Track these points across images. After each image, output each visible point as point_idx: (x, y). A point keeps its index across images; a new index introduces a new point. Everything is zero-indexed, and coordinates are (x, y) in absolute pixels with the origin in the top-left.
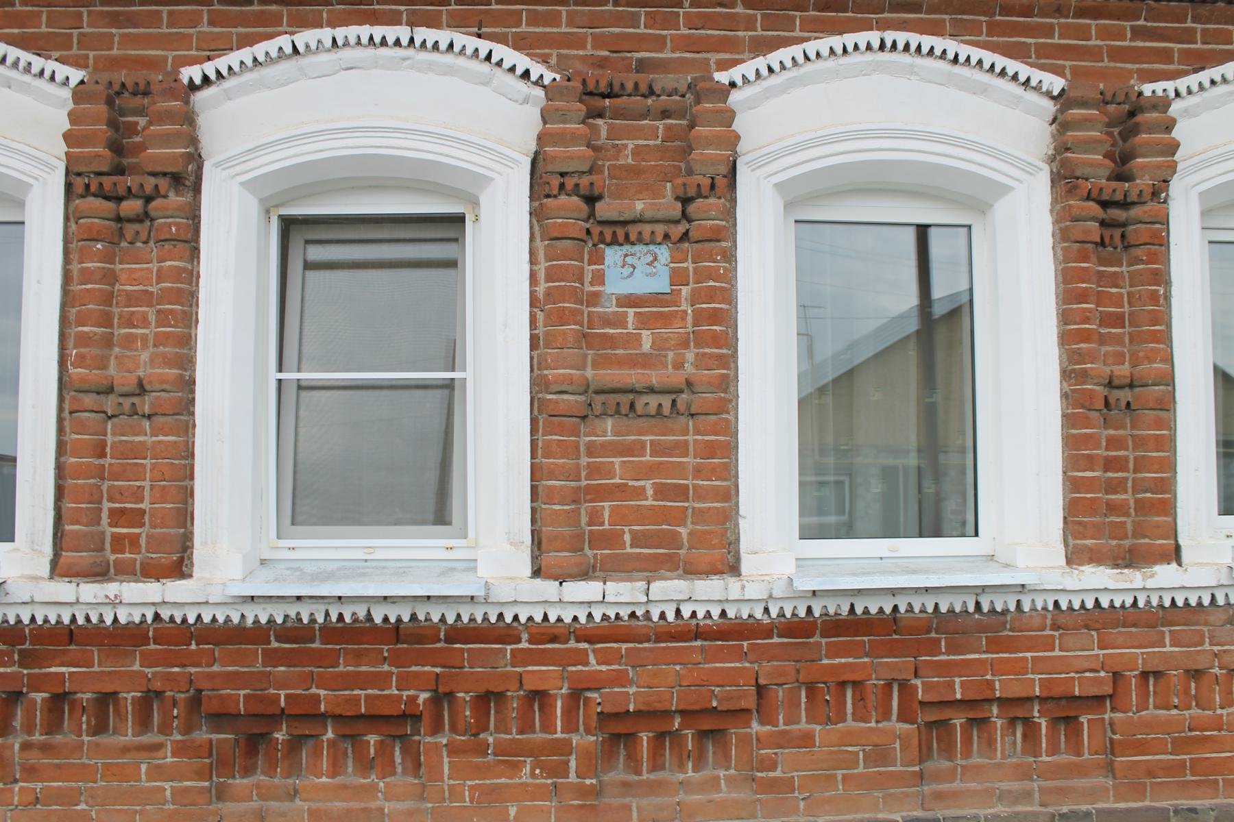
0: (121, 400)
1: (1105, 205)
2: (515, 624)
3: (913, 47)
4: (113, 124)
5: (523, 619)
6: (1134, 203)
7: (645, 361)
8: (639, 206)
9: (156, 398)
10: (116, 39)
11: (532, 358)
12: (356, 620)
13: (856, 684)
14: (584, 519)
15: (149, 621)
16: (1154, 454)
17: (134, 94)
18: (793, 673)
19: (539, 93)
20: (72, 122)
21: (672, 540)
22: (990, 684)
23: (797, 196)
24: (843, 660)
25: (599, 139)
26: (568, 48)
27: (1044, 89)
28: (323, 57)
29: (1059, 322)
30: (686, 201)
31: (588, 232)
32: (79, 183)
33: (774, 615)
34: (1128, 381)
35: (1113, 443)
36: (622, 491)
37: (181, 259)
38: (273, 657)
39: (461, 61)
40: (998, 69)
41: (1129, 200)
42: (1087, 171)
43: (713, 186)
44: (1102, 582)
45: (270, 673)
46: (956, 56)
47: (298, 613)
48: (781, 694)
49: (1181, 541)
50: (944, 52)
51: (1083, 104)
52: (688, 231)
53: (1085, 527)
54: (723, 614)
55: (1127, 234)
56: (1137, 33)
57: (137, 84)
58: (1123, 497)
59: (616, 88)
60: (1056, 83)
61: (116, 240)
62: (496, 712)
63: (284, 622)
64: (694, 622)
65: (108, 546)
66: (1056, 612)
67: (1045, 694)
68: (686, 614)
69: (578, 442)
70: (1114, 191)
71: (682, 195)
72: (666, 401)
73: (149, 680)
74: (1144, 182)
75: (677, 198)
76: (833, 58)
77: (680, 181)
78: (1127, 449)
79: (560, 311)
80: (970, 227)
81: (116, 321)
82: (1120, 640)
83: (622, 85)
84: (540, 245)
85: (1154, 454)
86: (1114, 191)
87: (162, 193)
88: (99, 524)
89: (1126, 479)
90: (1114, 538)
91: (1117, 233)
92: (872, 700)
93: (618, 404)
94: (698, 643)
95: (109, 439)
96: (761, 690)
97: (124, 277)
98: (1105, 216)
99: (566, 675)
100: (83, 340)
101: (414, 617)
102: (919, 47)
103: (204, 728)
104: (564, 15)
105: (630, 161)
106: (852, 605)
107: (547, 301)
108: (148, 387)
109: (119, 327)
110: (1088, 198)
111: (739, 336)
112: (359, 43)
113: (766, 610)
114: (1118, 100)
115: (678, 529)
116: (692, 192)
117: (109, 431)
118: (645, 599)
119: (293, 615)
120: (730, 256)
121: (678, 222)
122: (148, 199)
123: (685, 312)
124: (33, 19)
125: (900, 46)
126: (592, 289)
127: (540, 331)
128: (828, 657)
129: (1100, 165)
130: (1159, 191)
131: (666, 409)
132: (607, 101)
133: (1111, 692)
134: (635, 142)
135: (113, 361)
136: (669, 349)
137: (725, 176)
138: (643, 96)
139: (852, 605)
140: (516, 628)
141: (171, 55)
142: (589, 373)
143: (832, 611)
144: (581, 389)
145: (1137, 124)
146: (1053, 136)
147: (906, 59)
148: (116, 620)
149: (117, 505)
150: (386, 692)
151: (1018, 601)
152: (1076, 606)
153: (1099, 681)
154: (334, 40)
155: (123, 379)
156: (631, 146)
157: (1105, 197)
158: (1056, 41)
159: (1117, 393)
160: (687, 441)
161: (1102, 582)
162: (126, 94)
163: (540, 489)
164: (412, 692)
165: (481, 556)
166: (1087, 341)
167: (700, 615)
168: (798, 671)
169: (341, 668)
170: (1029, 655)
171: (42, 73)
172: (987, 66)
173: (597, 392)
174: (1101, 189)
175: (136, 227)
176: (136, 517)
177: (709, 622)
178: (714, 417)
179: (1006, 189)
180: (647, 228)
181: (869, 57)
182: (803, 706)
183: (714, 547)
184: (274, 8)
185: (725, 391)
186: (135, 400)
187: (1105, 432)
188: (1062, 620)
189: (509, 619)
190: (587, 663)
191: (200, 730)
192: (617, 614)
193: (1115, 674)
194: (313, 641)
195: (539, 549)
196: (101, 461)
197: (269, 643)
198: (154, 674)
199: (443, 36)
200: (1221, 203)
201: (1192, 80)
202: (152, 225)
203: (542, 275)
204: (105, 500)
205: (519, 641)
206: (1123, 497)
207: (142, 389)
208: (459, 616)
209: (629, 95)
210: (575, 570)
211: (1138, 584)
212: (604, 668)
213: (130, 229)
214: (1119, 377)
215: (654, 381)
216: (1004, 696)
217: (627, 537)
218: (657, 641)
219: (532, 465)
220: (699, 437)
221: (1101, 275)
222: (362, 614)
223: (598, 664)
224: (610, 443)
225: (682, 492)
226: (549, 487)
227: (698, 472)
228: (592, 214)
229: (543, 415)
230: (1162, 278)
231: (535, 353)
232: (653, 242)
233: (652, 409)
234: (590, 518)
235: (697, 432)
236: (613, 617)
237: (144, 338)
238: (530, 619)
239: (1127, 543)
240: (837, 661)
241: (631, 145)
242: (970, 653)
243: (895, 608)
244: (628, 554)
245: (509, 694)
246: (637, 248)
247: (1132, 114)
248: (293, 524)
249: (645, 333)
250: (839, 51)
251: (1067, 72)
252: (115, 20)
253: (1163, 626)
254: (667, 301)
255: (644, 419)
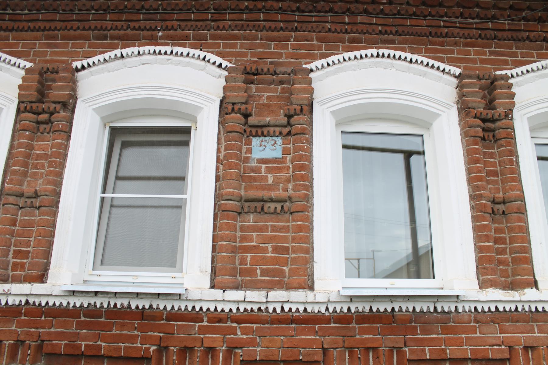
0: (27, 200)
1: (484, 121)
2: (201, 312)
3: (392, 56)
4: (40, 82)
5: (204, 309)
6: (497, 120)
7: (270, 188)
8: (268, 119)
9: (42, 199)
10: (49, 53)
11: (216, 186)
12: (123, 307)
13: (375, 349)
14: (237, 262)
15: (23, 304)
16: (519, 234)
17: (52, 73)
18: (341, 342)
19: (226, 73)
20: (23, 81)
21: (281, 273)
22: (444, 351)
23: (342, 119)
24: (367, 336)
25: (252, 92)
26: (240, 57)
27: (452, 73)
28: (134, 59)
29: (467, 173)
30: (289, 117)
31: (245, 131)
32: (22, 106)
33: (331, 311)
34: (502, 200)
35: (497, 230)
36: (256, 249)
37: (62, 139)
38: (81, 325)
39: (193, 60)
40: (430, 65)
41: (494, 118)
42: (474, 105)
43: (301, 110)
44: (497, 297)
45: (79, 333)
46: (411, 59)
47: (95, 303)
48: (335, 353)
49: (537, 278)
50: (406, 58)
51: (469, 77)
52: (290, 131)
53: (487, 269)
54: (305, 310)
55: (495, 135)
56: (491, 53)
57: (54, 68)
58: (505, 257)
59: (260, 71)
60: (457, 71)
61: (35, 131)
62: (189, 358)
63: (88, 307)
64: (290, 314)
65: (10, 268)
66: (476, 313)
67: (474, 357)
68: (286, 309)
69: (236, 225)
70: (487, 114)
71: (287, 114)
72: (279, 206)
73: (19, 335)
74: (501, 110)
75: (286, 115)
76: (356, 60)
77: (287, 108)
78: (505, 234)
79: (230, 164)
80: (422, 135)
81: (30, 166)
82: (511, 329)
83: (262, 69)
84: (222, 136)
85: (519, 234)
86: (487, 114)
87: (57, 110)
88: (7, 257)
89: (506, 248)
90: (503, 277)
91: (491, 134)
92: (382, 358)
93: (256, 207)
94: (293, 325)
95: (19, 218)
96: (325, 351)
97: (37, 147)
98: (484, 126)
99: (225, 340)
100: (14, 172)
101: (151, 306)
102: (394, 56)
103: (43, 362)
104: (239, 44)
105: (265, 101)
106: (371, 307)
107: (224, 159)
108: (39, 194)
109: (31, 169)
110: (475, 117)
111: (314, 177)
112: (149, 53)
113: (327, 309)
114: (486, 78)
115: (284, 268)
116: (292, 112)
117: (19, 214)
118: (265, 300)
119: (92, 303)
120: (310, 142)
121: (286, 126)
122: (52, 114)
123: (289, 167)
124: (17, 45)
125: (386, 55)
126: (246, 156)
127: (221, 174)
128: (359, 335)
129: (479, 102)
130: (508, 115)
131: (279, 210)
132: (255, 77)
133: (508, 357)
134: (265, 95)
135: (26, 183)
136: (281, 183)
137: (307, 105)
138: (271, 74)
139: (371, 307)
140: (201, 314)
141: (70, 59)
142: (243, 192)
143: (360, 310)
144: (238, 199)
145: (495, 85)
146: (457, 93)
147: (389, 61)
148: (7, 303)
149: (18, 249)
150: (135, 345)
151: (456, 307)
152: (486, 310)
153: (502, 351)
154: (139, 52)
155: (26, 188)
156: (266, 96)
157: (483, 117)
158: (456, 56)
159: (497, 206)
160: (288, 226)
161: (497, 297)
162: (49, 73)
163: (217, 247)
164: (147, 346)
165: (189, 278)
166: (481, 181)
167: (294, 310)
168: (344, 342)
169: (114, 332)
170: (464, 336)
171: (15, 64)
172: (425, 63)
173: (246, 201)
174: (481, 113)
175: (45, 126)
176: (25, 255)
177: (298, 314)
178: (301, 213)
179: (439, 115)
180: (272, 129)
181: (372, 60)
182: (347, 361)
183: (301, 276)
184: (116, 41)
185: (307, 202)
186: (33, 200)
187: (493, 226)
188: (480, 317)
189: (197, 309)
190: (236, 334)
191: (41, 362)
192: (252, 308)
193: (510, 347)
194: (101, 318)
195: (215, 276)
196: (14, 228)
197: (80, 318)
198: (21, 331)
199: (185, 50)
200: (538, 125)
201: (519, 70)
202: (52, 126)
203: (223, 149)
204: (12, 246)
205: (203, 321)
206: (505, 257)
207: (36, 195)
208: (173, 307)
209: (265, 74)
210: (231, 285)
211: (517, 299)
212: (244, 337)
213: (42, 127)
214: (498, 198)
215: (273, 195)
216: (452, 357)
217: (258, 271)
218: (272, 324)
219: (213, 235)
220: (294, 223)
221: (485, 153)
222: (126, 304)
223: (242, 334)
224: (251, 225)
225: (286, 250)
226: (221, 245)
227: (294, 239)
228: (246, 124)
229: (220, 211)
230: (514, 153)
231: (218, 184)
232: (274, 136)
233: (272, 210)
234: (241, 261)
235: (294, 221)
236: (249, 309)
237: (42, 174)
238: (208, 309)
239: (509, 280)
240: (364, 336)
241: (266, 95)
242: (433, 334)
243: (393, 309)
244: (259, 279)
245: (196, 348)
246: (267, 138)
247: (492, 83)
248: (102, 264)
249: (270, 176)
250: (359, 57)
251: (462, 68)
252: (49, 46)
253: (532, 322)
254: (280, 161)
255: (268, 215)
